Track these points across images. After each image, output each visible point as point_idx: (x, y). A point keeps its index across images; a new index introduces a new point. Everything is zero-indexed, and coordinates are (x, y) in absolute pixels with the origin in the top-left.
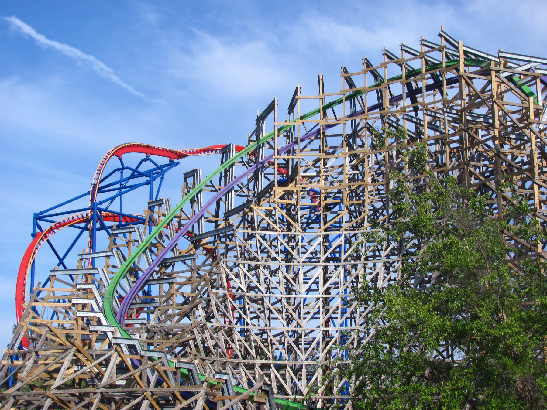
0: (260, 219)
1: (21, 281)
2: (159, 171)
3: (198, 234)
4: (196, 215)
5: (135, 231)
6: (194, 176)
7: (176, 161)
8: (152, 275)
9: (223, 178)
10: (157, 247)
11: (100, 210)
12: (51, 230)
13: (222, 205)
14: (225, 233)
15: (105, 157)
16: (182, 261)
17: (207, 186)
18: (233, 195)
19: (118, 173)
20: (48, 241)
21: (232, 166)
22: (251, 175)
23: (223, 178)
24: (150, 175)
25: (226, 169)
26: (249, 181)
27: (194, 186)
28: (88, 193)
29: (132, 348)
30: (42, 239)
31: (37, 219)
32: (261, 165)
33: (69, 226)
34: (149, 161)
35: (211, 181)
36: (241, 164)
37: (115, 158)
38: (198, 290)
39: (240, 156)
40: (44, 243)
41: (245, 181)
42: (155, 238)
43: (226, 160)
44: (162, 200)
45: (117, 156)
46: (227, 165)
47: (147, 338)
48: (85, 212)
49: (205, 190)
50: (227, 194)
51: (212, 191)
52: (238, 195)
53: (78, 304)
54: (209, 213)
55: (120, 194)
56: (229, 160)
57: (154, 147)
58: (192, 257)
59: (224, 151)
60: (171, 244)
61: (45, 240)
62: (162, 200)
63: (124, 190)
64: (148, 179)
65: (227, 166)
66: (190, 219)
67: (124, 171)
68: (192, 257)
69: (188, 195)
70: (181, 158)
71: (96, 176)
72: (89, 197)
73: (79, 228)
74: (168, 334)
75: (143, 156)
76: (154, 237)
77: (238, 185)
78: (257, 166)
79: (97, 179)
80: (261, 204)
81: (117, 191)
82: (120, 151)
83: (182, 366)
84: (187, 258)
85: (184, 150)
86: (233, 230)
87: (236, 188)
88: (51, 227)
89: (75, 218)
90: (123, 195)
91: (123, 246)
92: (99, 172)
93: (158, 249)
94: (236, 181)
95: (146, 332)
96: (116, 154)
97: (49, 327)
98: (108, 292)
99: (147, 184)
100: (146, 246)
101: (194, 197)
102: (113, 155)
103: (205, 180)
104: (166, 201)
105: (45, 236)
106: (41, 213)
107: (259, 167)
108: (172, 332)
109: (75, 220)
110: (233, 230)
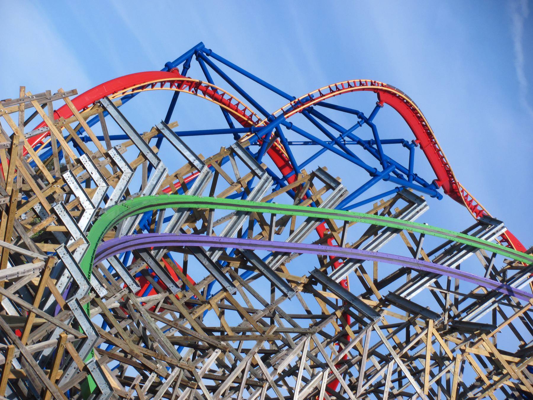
0: (422, 352)
1: (87, 99)
2: (405, 177)
3: (329, 275)
4: (355, 251)
5: (260, 178)
6: (411, 204)
7: (441, 191)
8: (213, 250)
9: (443, 250)
10: (263, 229)
11: (279, 134)
12: (196, 86)
13: (404, 279)
14: (364, 315)
15: (363, 81)
16: (273, 284)
17: (412, 236)
18: (428, 284)
19: (355, 119)
20: (177, 94)
21: (471, 249)
22: (482, 291)
23: (443, 250)
24: (388, 167)
25: (461, 244)
26: (472, 295)
27: (396, 216)
28: (290, 99)
29: (73, 287)
30: (172, 83)
31: (196, 52)
32: (506, 292)
33: (222, 109)
34: (408, 151)
35: (422, 235)
36: (485, 262)
37: (373, 98)
38: (244, 334)
39: (495, 251)
40: (169, 91)
41: (466, 288)
42: (273, 215)
43: (474, 235)
44: (338, 184)
45: (379, 97)
46: (469, 240)
47: (113, 310)
48: (260, 115)
49: (405, 239)
50: (422, 274)
51: (411, 249)
52: (433, 292)
53: (84, 168)
54: (375, 271)
55: (326, 147)
56: (476, 239)
57: (435, 143)
58: (285, 290)
59: (485, 221)
60: (281, 245)
61: (174, 89)
62: (338, 184)
63: (336, 146)
64: (380, 168)
65: (466, 243)
66: (341, 246)
67: (365, 125)
68: (285, 290)
69: (378, 217)
70: (450, 196)
71: (325, 89)
72: (287, 105)
73: (231, 124)
74: (143, 338)
75: (410, 137)
76: (274, 212)
77: (449, 282)
78: (500, 287)
79: (322, 95)
80: (448, 337)
81: (328, 139)
82: (390, 96)
83: (96, 374)
84: (283, 288)
85: (467, 191)
86: (372, 320)
87: (443, 282)
88: (200, 83)
89: (241, 108)
90: (328, 151)
91: (226, 178)
92: (334, 89)
93: (261, 234)
94: (451, 272)
95: (120, 303)
96: (381, 94)
97: (12, 143)
98: (136, 200)
99: (371, 174)
100: (249, 210)
101: (381, 227)
102: (375, 90)
103: (416, 224)
104: (340, 190)
105: (180, 85)
106: (210, 53)
107: (501, 291)
108: (150, 343)
109: (237, 110)
110: (372, 320)
